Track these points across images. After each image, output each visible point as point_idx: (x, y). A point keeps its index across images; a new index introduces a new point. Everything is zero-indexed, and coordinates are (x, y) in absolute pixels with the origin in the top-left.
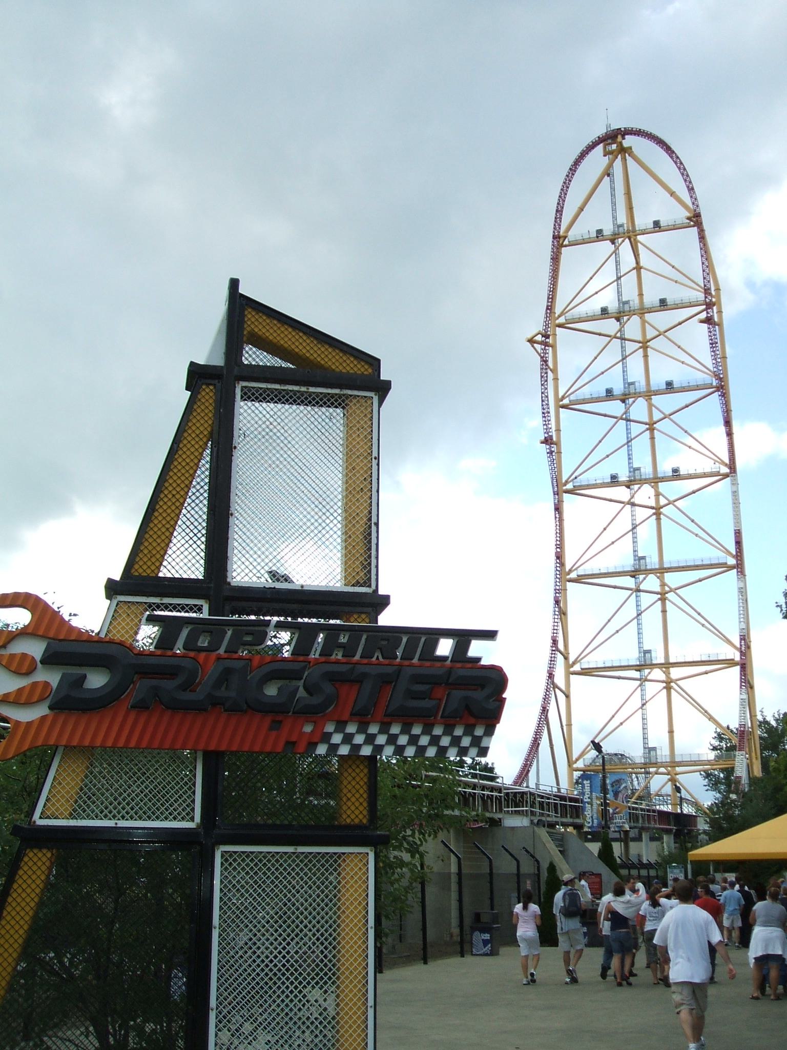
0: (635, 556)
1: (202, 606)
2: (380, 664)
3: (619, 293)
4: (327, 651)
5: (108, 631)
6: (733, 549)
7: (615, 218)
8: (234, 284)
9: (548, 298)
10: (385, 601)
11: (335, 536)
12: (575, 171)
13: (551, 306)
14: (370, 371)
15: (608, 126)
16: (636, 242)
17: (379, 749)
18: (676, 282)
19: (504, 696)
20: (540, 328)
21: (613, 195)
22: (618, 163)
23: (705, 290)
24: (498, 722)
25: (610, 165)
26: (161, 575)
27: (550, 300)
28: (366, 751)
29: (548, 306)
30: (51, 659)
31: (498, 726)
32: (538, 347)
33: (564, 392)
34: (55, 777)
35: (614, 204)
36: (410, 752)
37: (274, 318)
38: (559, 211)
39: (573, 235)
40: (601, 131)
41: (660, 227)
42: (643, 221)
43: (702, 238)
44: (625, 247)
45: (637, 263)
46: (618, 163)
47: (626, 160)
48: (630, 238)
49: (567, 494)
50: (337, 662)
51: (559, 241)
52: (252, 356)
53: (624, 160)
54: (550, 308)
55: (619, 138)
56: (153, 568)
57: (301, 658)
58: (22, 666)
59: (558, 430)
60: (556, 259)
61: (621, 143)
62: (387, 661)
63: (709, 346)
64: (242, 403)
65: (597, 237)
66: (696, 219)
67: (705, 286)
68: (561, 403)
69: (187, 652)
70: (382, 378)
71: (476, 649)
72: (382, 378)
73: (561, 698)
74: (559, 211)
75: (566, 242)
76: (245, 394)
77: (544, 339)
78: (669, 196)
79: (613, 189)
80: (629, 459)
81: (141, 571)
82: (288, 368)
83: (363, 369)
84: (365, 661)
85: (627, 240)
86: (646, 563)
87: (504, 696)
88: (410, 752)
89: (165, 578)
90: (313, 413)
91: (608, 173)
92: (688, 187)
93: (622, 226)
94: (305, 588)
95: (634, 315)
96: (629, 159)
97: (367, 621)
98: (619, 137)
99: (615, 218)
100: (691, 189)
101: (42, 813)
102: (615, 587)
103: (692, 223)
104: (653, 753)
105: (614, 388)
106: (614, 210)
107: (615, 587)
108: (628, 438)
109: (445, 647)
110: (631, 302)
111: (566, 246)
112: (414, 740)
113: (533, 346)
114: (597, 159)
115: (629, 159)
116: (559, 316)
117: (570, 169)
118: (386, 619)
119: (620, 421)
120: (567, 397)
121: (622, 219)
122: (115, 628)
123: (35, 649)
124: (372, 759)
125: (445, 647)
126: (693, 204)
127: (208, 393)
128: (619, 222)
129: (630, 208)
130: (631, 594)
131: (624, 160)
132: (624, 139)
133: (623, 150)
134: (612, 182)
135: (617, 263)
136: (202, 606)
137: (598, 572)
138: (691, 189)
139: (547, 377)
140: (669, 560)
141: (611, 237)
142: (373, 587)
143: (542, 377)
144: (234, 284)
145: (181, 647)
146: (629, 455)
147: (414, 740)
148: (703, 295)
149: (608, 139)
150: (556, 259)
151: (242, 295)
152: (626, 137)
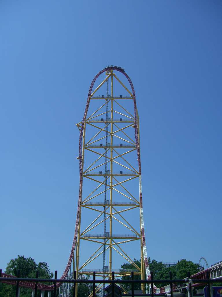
3: (107, 116)
38: (91, 88)
39: (94, 96)
41: (122, 97)
43: (135, 102)
53: (112, 77)
60: (89, 102)
65: (102, 98)
66: (134, 97)
68: (86, 121)
74: (91, 88)
75: (92, 98)
91: (107, 80)
99: (108, 93)
100: (133, 88)
102: (95, 242)
107: (95, 242)
111: (92, 99)
114: (105, 76)
116: (87, 120)
131: (112, 77)
133: (112, 75)
138: (133, 88)
143: (80, 139)
150: (89, 102)
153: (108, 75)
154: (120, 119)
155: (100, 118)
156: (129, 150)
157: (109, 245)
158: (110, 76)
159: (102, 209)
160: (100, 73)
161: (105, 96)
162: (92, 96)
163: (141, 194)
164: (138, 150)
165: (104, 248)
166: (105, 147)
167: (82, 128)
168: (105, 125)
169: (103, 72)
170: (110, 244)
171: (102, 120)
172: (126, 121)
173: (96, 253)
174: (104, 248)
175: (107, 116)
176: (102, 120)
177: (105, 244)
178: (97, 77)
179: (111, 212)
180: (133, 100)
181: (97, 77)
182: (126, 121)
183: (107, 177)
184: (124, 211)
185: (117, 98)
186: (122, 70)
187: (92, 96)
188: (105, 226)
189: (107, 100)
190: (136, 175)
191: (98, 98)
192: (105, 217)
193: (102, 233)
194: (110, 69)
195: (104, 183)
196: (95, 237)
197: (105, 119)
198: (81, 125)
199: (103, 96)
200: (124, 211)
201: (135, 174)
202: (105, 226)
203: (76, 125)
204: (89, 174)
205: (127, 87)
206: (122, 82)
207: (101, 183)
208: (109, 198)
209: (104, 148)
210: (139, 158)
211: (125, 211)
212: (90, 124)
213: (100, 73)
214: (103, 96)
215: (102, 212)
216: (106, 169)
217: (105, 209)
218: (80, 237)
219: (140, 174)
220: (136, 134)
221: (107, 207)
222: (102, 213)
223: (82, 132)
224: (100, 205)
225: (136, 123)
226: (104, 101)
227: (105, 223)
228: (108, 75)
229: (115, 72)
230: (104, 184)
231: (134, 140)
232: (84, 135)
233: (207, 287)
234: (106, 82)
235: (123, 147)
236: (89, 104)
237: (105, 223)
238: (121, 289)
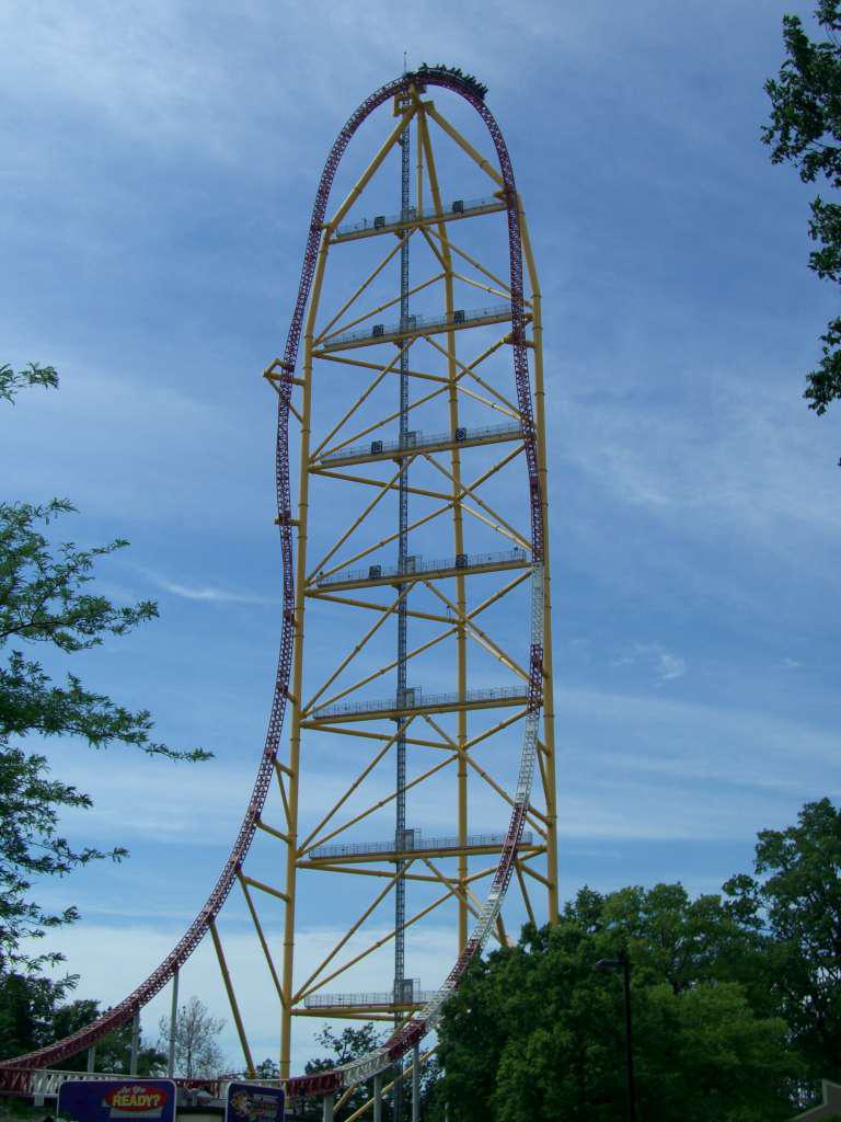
0: (399, 688)
18: (478, 380)
22: (414, 124)
25: (403, 129)
27: (299, 312)
32: (277, 383)
33: (321, 332)
41: (462, 211)
46: (414, 124)
49: (308, 730)
59: (304, 505)
66: (509, 198)
68: (314, 349)
73: (286, 779)
74: (323, 193)
75: (334, 237)
77: (285, 372)
78: (478, 167)
79: (405, 162)
91: (400, 138)
99: (405, 201)
100: (503, 156)
104: (408, 838)
108: (401, 528)
110: (417, 435)
111: (334, 242)
113: (272, 383)
116: (318, 342)
119: (389, 373)
120: (307, 851)
130: (390, 745)
131: (423, 123)
133: (427, 108)
134: (405, 152)
137: (347, 580)
138: (503, 156)
141: (395, 455)
159: (390, 728)
160: (362, 115)
167: (284, 377)
186: (473, 91)
191: (217, 903)
198: (278, 371)
205: (453, 523)
212: (330, 358)
218: (314, 349)
222: (388, 742)
226: (392, 240)
229: (433, 93)
230: (396, 371)
233: (528, 949)
237: (400, 950)
238: (460, 572)
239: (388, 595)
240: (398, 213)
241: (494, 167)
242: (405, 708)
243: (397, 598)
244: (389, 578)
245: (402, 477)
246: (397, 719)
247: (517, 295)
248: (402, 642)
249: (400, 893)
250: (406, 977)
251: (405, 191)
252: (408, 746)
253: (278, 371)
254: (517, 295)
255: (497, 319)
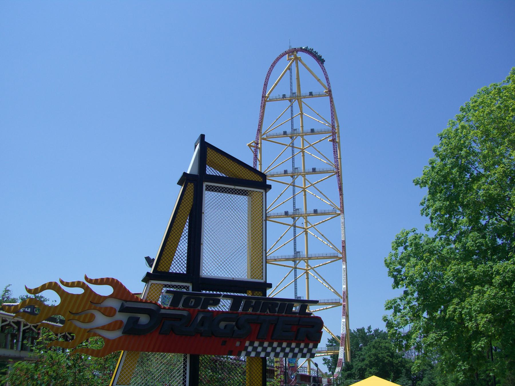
1: (189, 286)
2: (269, 315)
3: (292, 125)
4: (245, 308)
5: (147, 297)
6: (341, 250)
7: (291, 89)
8: (202, 137)
9: (259, 126)
10: (270, 286)
11: (185, 242)
12: (274, 67)
13: (260, 129)
14: (261, 180)
15: (290, 47)
16: (301, 101)
17: (268, 354)
19: (322, 331)
20: (254, 139)
21: (291, 79)
23: (332, 126)
24: (320, 343)
26: (171, 271)
28: (263, 355)
29: (258, 129)
30: (123, 310)
31: (319, 344)
34: (123, 365)
35: (291, 83)
36: (253, 354)
37: (218, 152)
38: (266, 85)
39: (271, 96)
40: (287, 49)
41: (312, 95)
42: (305, 91)
43: (331, 101)
44: (296, 104)
45: (301, 111)
47: (298, 63)
48: (298, 100)
50: (251, 314)
51: (264, 99)
52: (210, 171)
53: (297, 63)
54: (259, 130)
55: (295, 53)
56: (167, 267)
57: (235, 312)
58: (109, 312)
60: (263, 107)
61: (296, 55)
62: (272, 314)
63: (333, 152)
64: (206, 192)
65: (283, 98)
67: (332, 124)
68: (262, 137)
69: (185, 308)
70: (267, 184)
71: (312, 309)
72: (267, 184)
74: (266, 85)
75: (268, 99)
76: (207, 188)
79: (291, 76)
80: (294, 204)
81: (161, 269)
82: (223, 176)
83: (260, 179)
84: (263, 313)
85: (297, 100)
86: (300, 254)
87: (322, 331)
88: (253, 354)
89: (172, 273)
90: (231, 197)
91: (289, 69)
92: (326, 77)
93: (295, 93)
94: (234, 279)
95: (299, 136)
96: (299, 62)
97: (261, 294)
98: (295, 52)
99: (291, 89)
100: (327, 79)
101: (117, 382)
102: (285, 266)
103: (327, 94)
105: (288, 170)
106: (291, 86)
107: (285, 266)
109: (296, 309)
111: (268, 101)
112: (255, 349)
113: (250, 148)
114: (285, 62)
115: (299, 62)
116: (264, 134)
117: (272, 65)
118: (270, 293)
121: (295, 90)
122: (150, 296)
123: (116, 304)
124: (264, 360)
125: (296, 309)
126: (328, 85)
127: (191, 187)
128: (293, 91)
129: (299, 85)
131: (297, 63)
132: (297, 53)
133: (296, 59)
134: (291, 72)
135: (292, 111)
136: (189, 286)
138: (327, 79)
139: (256, 163)
140: (311, 253)
142: (264, 280)
143: (254, 163)
144: (202, 137)
145: (181, 306)
146: (294, 202)
147: (255, 349)
148: (331, 128)
149: (290, 52)
150: (263, 107)
151: (206, 142)
152: (298, 52)
153: (289, 60)
154: (311, 129)
155: (281, 170)
156: (327, 176)
157: (305, 270)
158: (293, 61)
159: (291, 264)
160: (278, 59)
161: (288, 94)
162: (268, 97)
163: (344, 242)
164: (339, 175)
165: (295, 275)
166: (289, 98)
168: (290, 104)
169: (282, 56)
170: (306, 268)
171: (285, 133)
172: (320, 133)
173: (285, 278)
174: (295, 275)
175: (292, 125)
176: (285, 133)
177: (296, 268)
178: (273, 66)
179: (307, 226)
180: (328, 98)
181: (273, 66)
182: (321, 133)
183: (297, 218)
184: (323, 265)
185: (304, 97)
186: (320, 60)
187: (268, 97)
188: (296, 289)
189: (290, 101)
190: (337, 213)
191: (276, 100)
192: (293, 151)
193: (291, 253)
194: (292, 52)
195: (291, 145)
196: (282, 259)
197: (289, 131)
198: (253, 144)
199: (284, 96)
200: (323, 265)
201: (336, 212)
202: (296, 289)
203: (247, 145)
204: (270, 216)
206: (310, 69)
207: (287, 145)
208: (301, 248)
209: (289, 136)
210: (341, 189)
211: (325, 264)
213: (278, 59)
214: (284, 96)
215: (288, 184)
216: (294, 207)
217: (295, 264)
219: (342, 211)
220: (335, 152)
221: (297, 262)
223: (256, 156)
224: (287, 259)
225: (334, 133)
227: (296, 284)
228: (289, 60)
229: (300, 54)
230: (290, 146)
231: (333, 160)
232: (259, 159)
234: (288, 71)
235: (317, 173)
236: (263, 112)
237: (296, 284)
239: (290, 221)
240: (292, 170)
241: (325, 84)
242: (296, 258)
243: (292, 181)
244: (291, 215)
245: (293, 143)
246: (294, 261)
247: (333, 126)
248: (292, 114)
249: (295, 271)
250: (297, 251)
251: (291, 86)
252: (297, 270)
253: (253, 144)
254: (333, 126)
255: (325, 132)
